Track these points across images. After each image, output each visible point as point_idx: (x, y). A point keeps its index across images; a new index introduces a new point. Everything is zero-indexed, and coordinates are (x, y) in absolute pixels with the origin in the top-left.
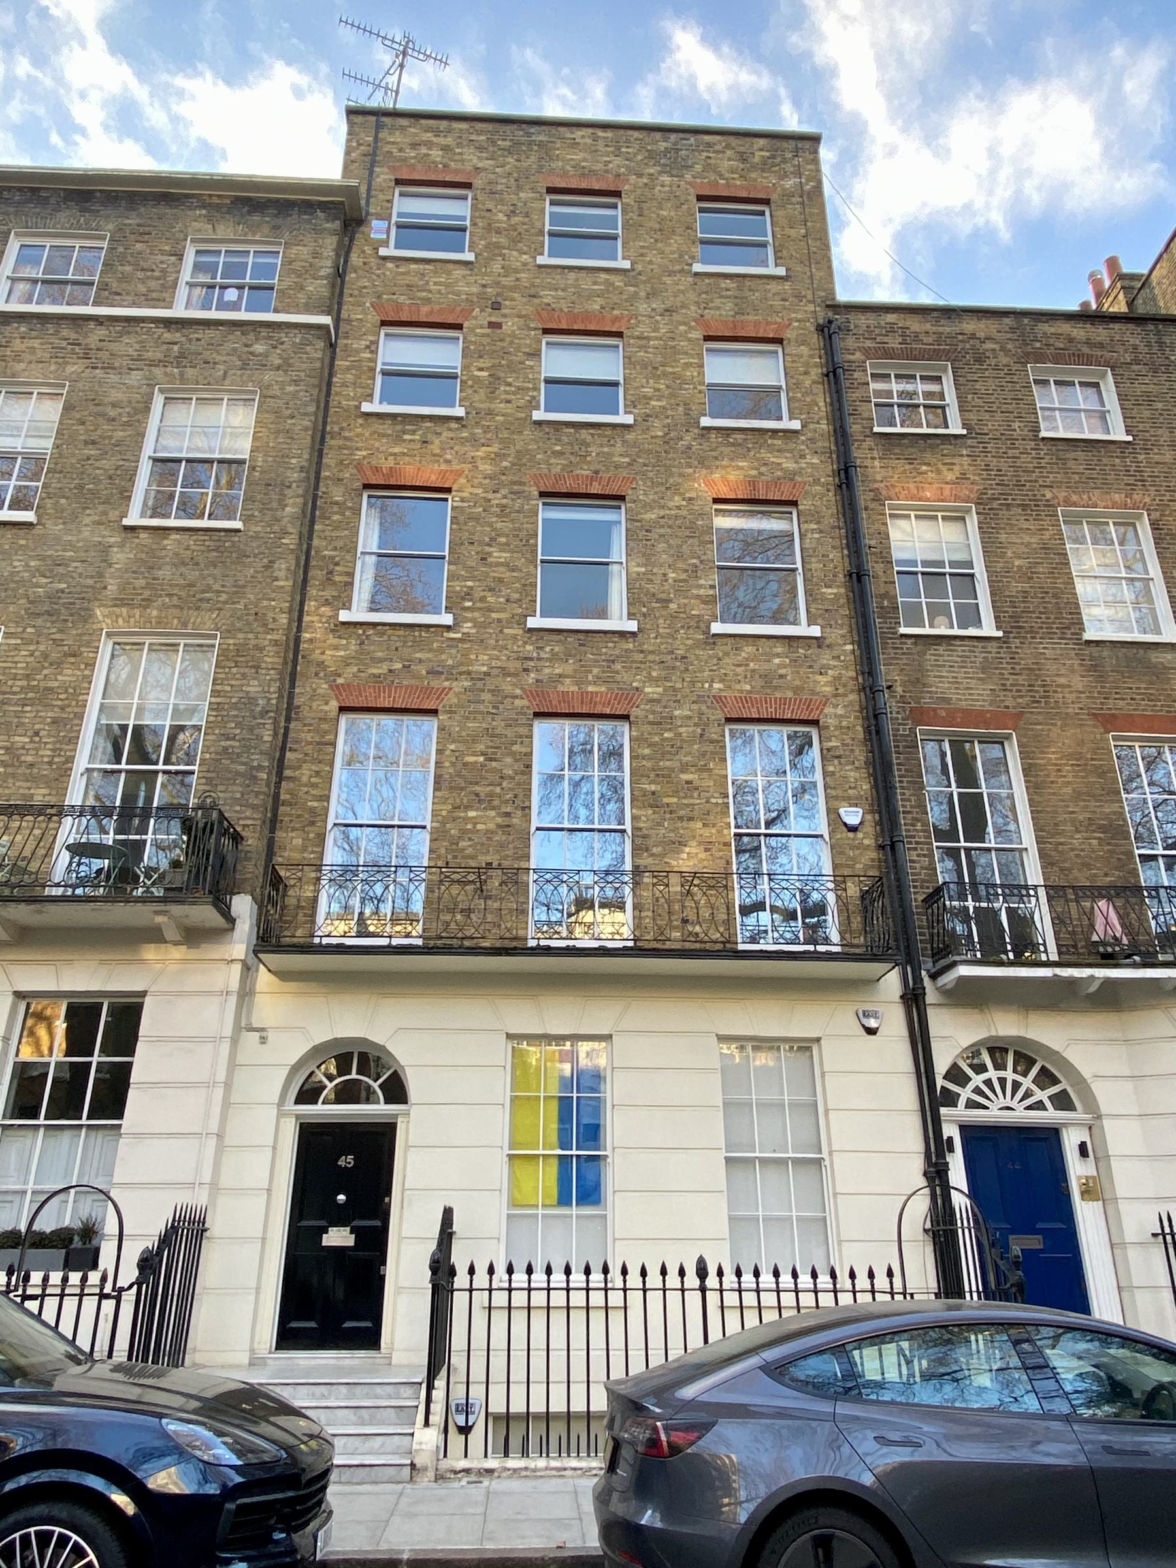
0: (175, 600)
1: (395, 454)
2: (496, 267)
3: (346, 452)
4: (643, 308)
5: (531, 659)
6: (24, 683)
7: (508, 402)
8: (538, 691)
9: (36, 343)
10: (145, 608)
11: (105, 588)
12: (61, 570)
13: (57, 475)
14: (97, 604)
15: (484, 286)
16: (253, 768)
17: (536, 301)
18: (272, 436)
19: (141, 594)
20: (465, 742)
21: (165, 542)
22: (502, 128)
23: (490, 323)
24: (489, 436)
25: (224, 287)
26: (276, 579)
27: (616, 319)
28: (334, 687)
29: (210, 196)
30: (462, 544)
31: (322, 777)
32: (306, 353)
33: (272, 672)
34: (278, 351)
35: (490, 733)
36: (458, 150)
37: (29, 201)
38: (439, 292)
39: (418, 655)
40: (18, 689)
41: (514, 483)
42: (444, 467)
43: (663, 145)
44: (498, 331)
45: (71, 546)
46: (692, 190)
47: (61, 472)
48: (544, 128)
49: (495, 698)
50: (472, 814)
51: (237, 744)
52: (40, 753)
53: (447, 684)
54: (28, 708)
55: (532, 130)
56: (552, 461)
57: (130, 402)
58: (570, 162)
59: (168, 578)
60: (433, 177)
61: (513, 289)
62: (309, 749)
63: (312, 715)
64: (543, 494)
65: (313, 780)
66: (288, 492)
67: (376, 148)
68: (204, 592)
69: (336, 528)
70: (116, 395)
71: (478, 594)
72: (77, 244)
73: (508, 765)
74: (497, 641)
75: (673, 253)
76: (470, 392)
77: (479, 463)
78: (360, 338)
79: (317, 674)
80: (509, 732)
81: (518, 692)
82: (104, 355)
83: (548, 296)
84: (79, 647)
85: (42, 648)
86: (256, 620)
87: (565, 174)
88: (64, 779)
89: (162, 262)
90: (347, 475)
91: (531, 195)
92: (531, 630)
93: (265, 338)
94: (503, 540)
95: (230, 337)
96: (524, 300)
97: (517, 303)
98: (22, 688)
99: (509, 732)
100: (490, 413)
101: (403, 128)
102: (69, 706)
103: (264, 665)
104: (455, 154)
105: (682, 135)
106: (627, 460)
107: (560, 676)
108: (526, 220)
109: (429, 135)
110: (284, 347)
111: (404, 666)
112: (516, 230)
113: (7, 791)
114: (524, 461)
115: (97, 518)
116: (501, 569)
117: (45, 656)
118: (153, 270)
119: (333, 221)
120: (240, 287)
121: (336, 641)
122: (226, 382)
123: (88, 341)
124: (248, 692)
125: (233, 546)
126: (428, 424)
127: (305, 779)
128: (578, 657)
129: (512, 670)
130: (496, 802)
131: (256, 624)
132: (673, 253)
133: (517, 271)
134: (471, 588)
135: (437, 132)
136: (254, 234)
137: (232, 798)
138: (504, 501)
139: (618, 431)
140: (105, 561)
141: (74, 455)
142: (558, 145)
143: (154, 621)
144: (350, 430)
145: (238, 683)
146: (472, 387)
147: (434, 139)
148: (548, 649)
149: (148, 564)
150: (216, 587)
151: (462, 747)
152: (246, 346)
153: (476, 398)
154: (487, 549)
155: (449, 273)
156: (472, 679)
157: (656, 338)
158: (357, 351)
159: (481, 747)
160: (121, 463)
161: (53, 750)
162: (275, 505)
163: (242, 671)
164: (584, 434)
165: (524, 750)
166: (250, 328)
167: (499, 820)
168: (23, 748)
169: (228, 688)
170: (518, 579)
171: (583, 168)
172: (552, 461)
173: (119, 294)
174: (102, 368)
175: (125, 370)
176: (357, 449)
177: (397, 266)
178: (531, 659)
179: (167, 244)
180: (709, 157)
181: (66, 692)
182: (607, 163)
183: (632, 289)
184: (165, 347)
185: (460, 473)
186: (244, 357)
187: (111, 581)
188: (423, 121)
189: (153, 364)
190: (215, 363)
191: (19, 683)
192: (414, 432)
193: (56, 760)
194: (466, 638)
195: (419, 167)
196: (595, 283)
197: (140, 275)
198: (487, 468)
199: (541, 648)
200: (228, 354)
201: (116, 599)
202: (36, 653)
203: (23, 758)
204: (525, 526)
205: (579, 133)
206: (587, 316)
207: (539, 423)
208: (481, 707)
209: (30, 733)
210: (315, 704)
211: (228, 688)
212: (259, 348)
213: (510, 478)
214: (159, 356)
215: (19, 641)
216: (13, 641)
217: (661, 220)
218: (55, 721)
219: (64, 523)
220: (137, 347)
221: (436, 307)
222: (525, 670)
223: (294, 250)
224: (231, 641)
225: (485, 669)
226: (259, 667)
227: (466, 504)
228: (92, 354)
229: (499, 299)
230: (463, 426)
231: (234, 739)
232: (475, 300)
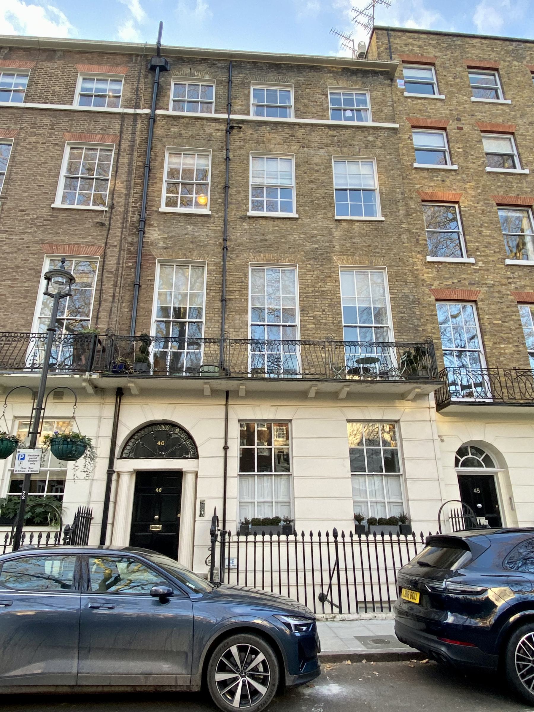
0: (364, 253)
1: (432, 186)
2: (454, 102)
3: (411, 185)
4: (520, 121)
5: (510, 278)
6: (313, 289)
7: (474, 163)
8: (517, 292)
9: (275, 135)
10: (353, 256)
11: (334, 247)
12: (314, 239)
13: (301, 197)
14: (333, 254)
15: (451, 110)
16: (415, 325)
17: (475, 117)
18: (386, 179)
19: (350, 250)
20: (491, 314)
21: (354, 227)
22: (441, 38)
23: (458, 127)
24: (469, 178)
25: (345, 110)
26: (404, 243)
27: (510, 126)
28: (431, 290)
29: (332, 67)
30: (469, 227)
31: (436, 329)
32: (391, 141)
33: (412, 284)
34: (379, 140)
35: (501, 310)
36: (425, 48)
37: (253, 68)
38: (433, 112)
39: (463, 276)
40: (311, 292)
41: (485, 199)
42: (454, 192)
43: (511, 48)
44: (462, 131)
45: (315, 228)
46: (527, 69)
47: (302, 195)
48: (459, 38)
49: (500, 295)
50: (502, 346)
51: (406, 315)
52: (327, 319)
53: (478, 289)
54: (317, 300)
55: (454, 39)
56: (498, 190)
57: (322, 163)
58: (476, 53)
59: (359, 242)
60: (418, 60)
61: (464, 112)
62: (427, 317)
63: (425, 302)
64: (498, 205)
65: (433, 331)
66: (399, 204)
67: (390, 46)
68: (375, 249)
69: (415, 220)
70: (316, 160)
71: (481, 249)
72: (278, 88)
73: (512, 325)
74: (494, 270)
75: (527, 97)
76: (457, 158)
77: (468, 190)
78: (404, 133)
79: (423, 285)
80: (509, 310)
81: (509, 292)
82: (306, 141)
83: (479, 116)
84: (331, 273)
85: (316, 273)
86: (399, 261)
87: (473, 60)
88: (340, 330)
89: (319, 98)
90: (414, 196)
91: (461, 69)
92: (508, 265)
93: (372, 134)
94: (486, 225)
95: (357, 133)
96: (470, 117)
97: (466, 118)
98: (312, 291)
99: (509, 310)
100: (467, 168)
101: (400, 37)
102: (334, 299)
103: (408, 281)
104: (424, 49)
105: (517, 43)
106: (529, 190)
107: (525, 285)
108: (462, 80)
109: (411, 40)
110: (381, 138)
111: (458, 281)
112: (458, 85)
113: (318, 335)
114: (487, 189)
115: (322, 216)
116: (488, 238)
117: (318, 277)
118: (316, 102)
119: (387, 80)
120: (352, 110)
121: (427, 270)
122: (361, 154)
123: (298, 134)
124: (405, 293)
125: (382, 228)
126: (443, 173)
127: (429, 330)
128: (530, 277)
129: (504, 283)
130: (511, 341)
131: (400, 263)
132: (527, 97)
133: (463, 104)
134: (478, 246)
135: (415, 39)
136: (356, 86)
137: (410, 339)
138: (483, 208)
139: (523, 177)
140: (331, 235)
141: (305, 187)
142: (467, 46)
143: (358, 261)
144: (410, 176)
145: (400, 289)
146: (457, 156)
147: (413, 42)
148: (516, 274)
149: (349, 236)
150: (380, 246)
151: (491, 317)
152: (365, 137)
153: (460, 161)
154: (481, 229)
155: (435, 104)
156: (488, 287)
157: (529, 136)
158: (405, 140)
159: (498, 317)
160: (327, 191)
161: (333, 318)
162: (395, 210)
163: (400, 283)
164: (509, 178)
165: (517, 318)
166: (365, 129)
167: (514, 348)
168: (320, 317)
169: (396, 291)
170: (497, 243)
171: (480, 57)
172: (498, 190)
173: (305, 113)
174: (307, 147)
175: (316, 148)
176: (416, 184)
177: (413, 101)
178: (510, 278)
179: (320, 90)
180: (531, 54)
181: (331, 293)
182: (490, 55)
183: (513, 113)
184: (331, 138)
185: (461, 195)
186: (366, 142)
187: (336, 244)
188: (407, 34)
189: (327, 145)
190: (354, 145)
191: (310, 289)
192: (437, 176)
193: (335, 322)
194: (481, 268)
195: (411, 55)
196: (497, 110)
197: (312, 104)
198: (472, 193)
199: (514, 273)
200: (358, 141)
201: (340, 252)
202: (314, 276)
203: (321, 321)
204: (494, 219)
205: (475, 41)
206: (498, 125)
207: (489, 173)
208: (494, 299)
209: (321, 310)
210: (425, 298)
211: (396, 291)
212: (371, 138)
213: (482, 197)
214: (329, 142)
215: (306, 271)
216: (303, 271)
217: (519, 82)
218: (329, 305)
219: (310, 218)
220: (319, 137)
221: (434, 120)
222: (509, 283)
223: (374, 93)
224: (392, 270)
225: (492, 282)
226: (406, 282)
227: (467, 209)
228: (301, 140)
229: (459, 117)
230: (458, 174)
231: (404, 313)
232: (449, 116)
